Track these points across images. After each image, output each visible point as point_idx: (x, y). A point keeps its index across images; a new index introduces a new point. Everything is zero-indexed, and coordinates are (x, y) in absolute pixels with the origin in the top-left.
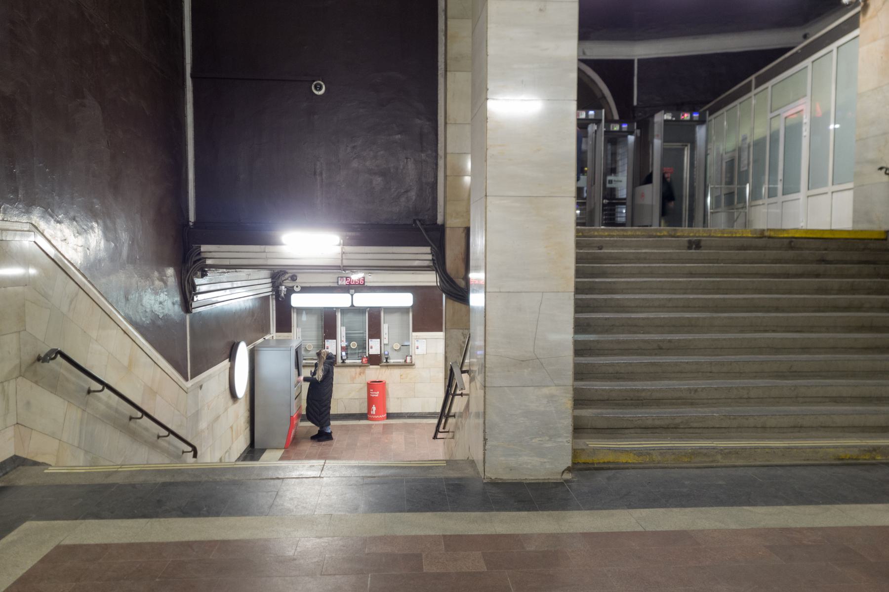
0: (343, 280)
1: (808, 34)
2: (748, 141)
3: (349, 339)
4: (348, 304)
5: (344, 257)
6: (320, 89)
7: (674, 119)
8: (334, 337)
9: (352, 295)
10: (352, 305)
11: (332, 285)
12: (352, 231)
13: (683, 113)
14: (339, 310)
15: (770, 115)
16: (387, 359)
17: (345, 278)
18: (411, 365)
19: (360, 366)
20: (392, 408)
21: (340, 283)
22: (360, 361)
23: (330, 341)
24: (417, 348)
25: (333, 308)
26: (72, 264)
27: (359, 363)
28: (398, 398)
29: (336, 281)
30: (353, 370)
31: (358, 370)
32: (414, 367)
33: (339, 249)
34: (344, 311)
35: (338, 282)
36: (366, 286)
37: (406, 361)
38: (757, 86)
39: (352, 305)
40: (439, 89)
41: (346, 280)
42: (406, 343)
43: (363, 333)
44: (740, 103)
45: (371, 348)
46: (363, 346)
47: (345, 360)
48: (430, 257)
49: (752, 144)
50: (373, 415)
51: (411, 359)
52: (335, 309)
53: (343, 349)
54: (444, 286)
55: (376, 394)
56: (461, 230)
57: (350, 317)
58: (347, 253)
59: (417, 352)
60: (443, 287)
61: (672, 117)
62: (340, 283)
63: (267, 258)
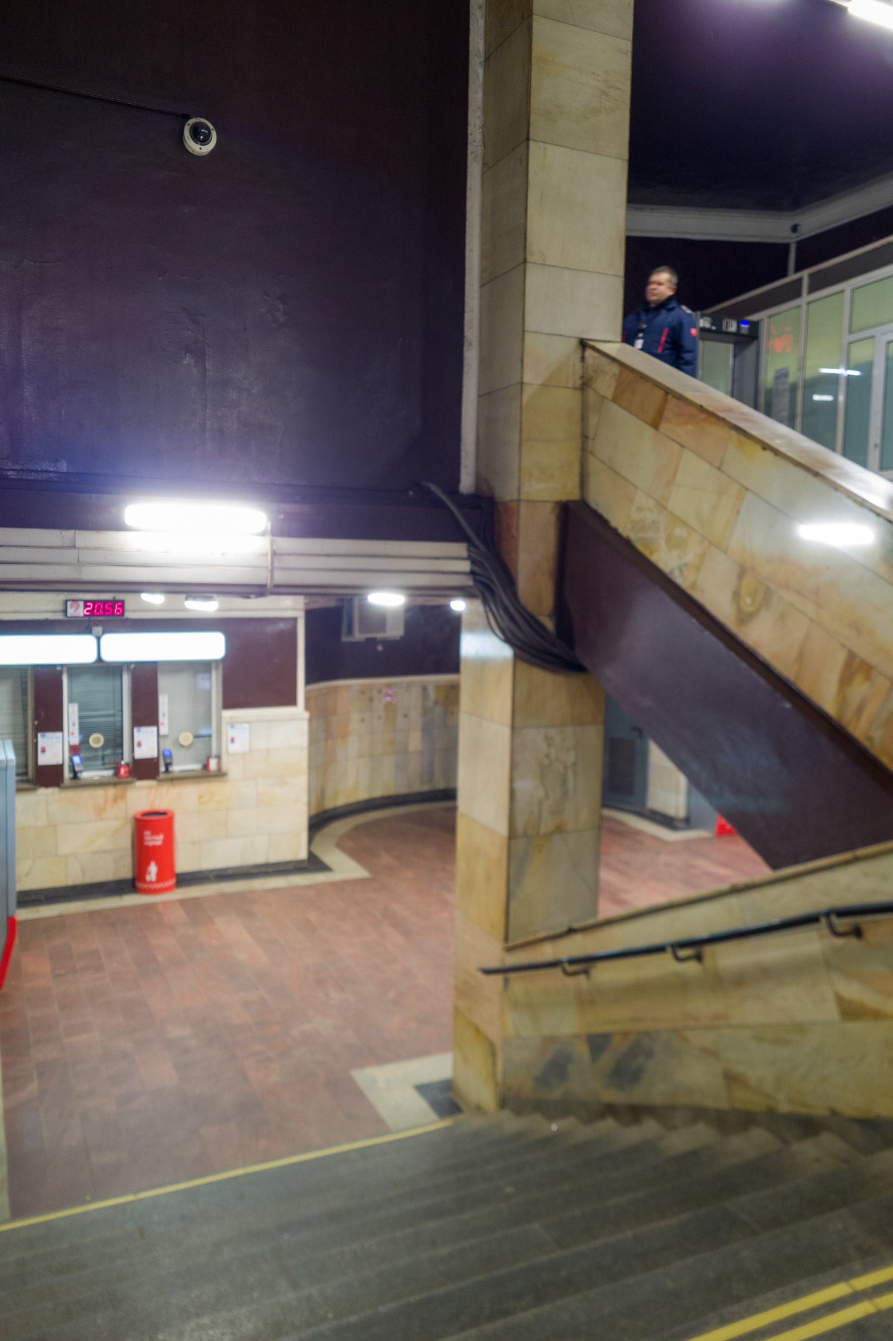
0: (78, 607)
1: (799, 225)
2: (792, 378)
3: (86, 730)
4: (89, 657)
5: (276, 564)
6: (205, 141)
7: (714, 328)
8: (57, 726)
9: (98, 639)
10: (99, 659)
11: (51, 616)
12: (296, 502)
13: (728, 320)
14: (65, 669)
15: (847, 338)
16: (167, 765)
17: (82, 604)
18: (220, 774)
19: (115, 784)
20: (183, 863)
21: (71, 612)
22: (110, 773)
23: (49, 735)
24: (233, 740)
25: (53, 666)
26: (260, 591)
27: (109, 777)
28: (194, 843)
29: (61, 607)
30: (100, 792)
31: (111, 791)
32: (226, 778)
33: (262, 545)
34: (76, 670)
35: (65, 611)
36: (127, 619)
37: (206, 767)
38: (812, 289)
39: (99, 659)
40: (468, 186)
41: (86, 606)
42: (203, 732)
43: (114, 715)
44: (770, 317)
45: (139, 744)
46: (115, 742)
47: (81, 772)
48: (466, 566)
49: (801, 384)
50: (151, 882)
51: (219, 764)
52: (59, 668)
53: (74, 750)
54: (516, 631)
55: (155, 840)
56: (549, 507)
57: (86, 683)
58: (282, 555)
59: (233, 748)
60: (512, 632)
61: (712, 324)
62: (71, 612)
63: (80, 564)
